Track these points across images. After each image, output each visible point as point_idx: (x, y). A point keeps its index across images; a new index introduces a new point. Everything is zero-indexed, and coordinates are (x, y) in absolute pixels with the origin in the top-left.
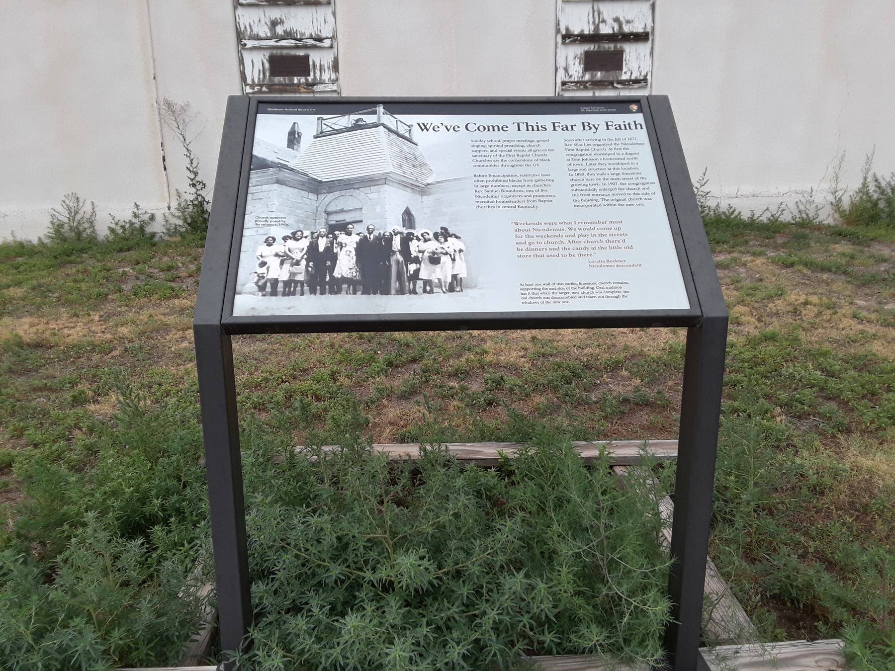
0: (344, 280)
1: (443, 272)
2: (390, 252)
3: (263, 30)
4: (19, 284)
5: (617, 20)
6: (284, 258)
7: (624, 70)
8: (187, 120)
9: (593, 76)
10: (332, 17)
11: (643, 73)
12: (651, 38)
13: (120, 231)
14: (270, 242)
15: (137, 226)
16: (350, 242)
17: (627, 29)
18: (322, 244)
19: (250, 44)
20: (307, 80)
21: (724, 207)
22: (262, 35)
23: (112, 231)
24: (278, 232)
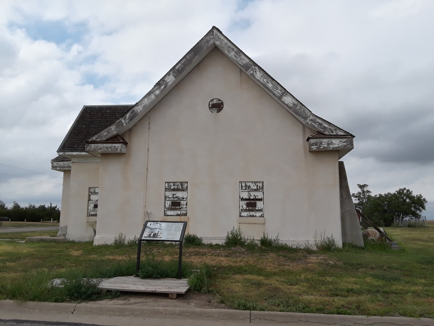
0: (151, 237)
1: (160, 236)
2: (156, 234)
3: (171, 196)
4: (108, 251)
5: (254, 196)
6: (147, 235)
7: (257, 207)
8: (151, 216)
9: (249, 208)
10: (187, 194)
11: (262, 208)
12: (263, 200)
13: (130, 243)
14: (146, 233)
15: (134, 241)
16: (153, 234)
17: (257, 198)
18: (150, 234)
19: (167, 199)
20: (179, 207)
21: (284, 243)
22: (170, 197)
23: (128, 242)
24: (147, 233)
